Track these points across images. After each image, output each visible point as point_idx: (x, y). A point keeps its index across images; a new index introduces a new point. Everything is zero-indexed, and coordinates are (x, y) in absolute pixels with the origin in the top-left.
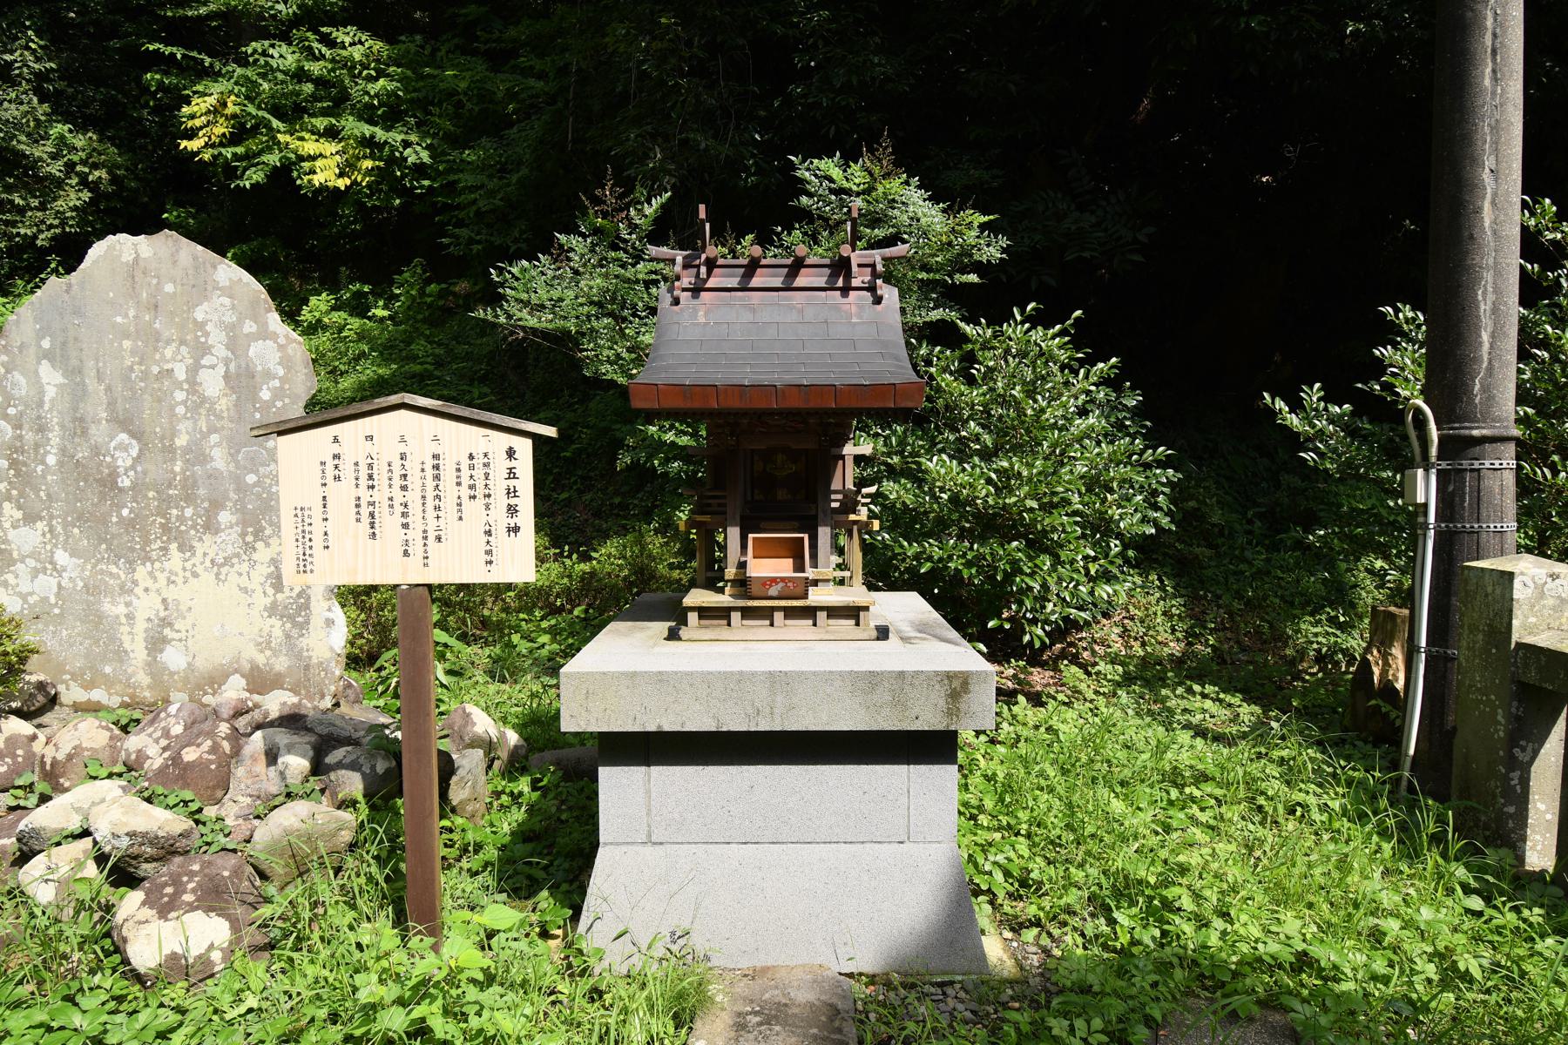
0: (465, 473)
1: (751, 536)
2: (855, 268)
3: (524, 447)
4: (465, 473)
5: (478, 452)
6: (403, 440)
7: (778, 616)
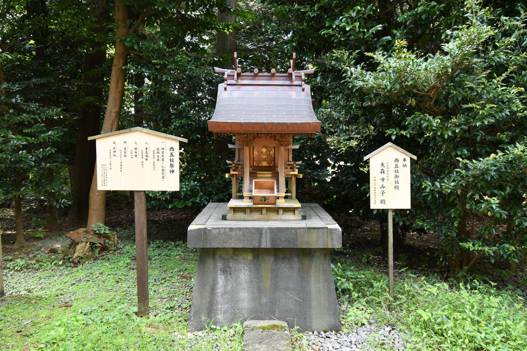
0: (156, 155)
1: (254, 180)
2: (294, 77)
3: (176, 146)
4: (156, 155)
5: (160, 147)
6: (125, 142)
7: (264, 211)
